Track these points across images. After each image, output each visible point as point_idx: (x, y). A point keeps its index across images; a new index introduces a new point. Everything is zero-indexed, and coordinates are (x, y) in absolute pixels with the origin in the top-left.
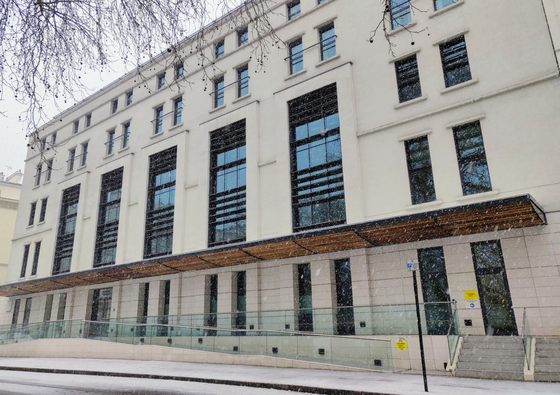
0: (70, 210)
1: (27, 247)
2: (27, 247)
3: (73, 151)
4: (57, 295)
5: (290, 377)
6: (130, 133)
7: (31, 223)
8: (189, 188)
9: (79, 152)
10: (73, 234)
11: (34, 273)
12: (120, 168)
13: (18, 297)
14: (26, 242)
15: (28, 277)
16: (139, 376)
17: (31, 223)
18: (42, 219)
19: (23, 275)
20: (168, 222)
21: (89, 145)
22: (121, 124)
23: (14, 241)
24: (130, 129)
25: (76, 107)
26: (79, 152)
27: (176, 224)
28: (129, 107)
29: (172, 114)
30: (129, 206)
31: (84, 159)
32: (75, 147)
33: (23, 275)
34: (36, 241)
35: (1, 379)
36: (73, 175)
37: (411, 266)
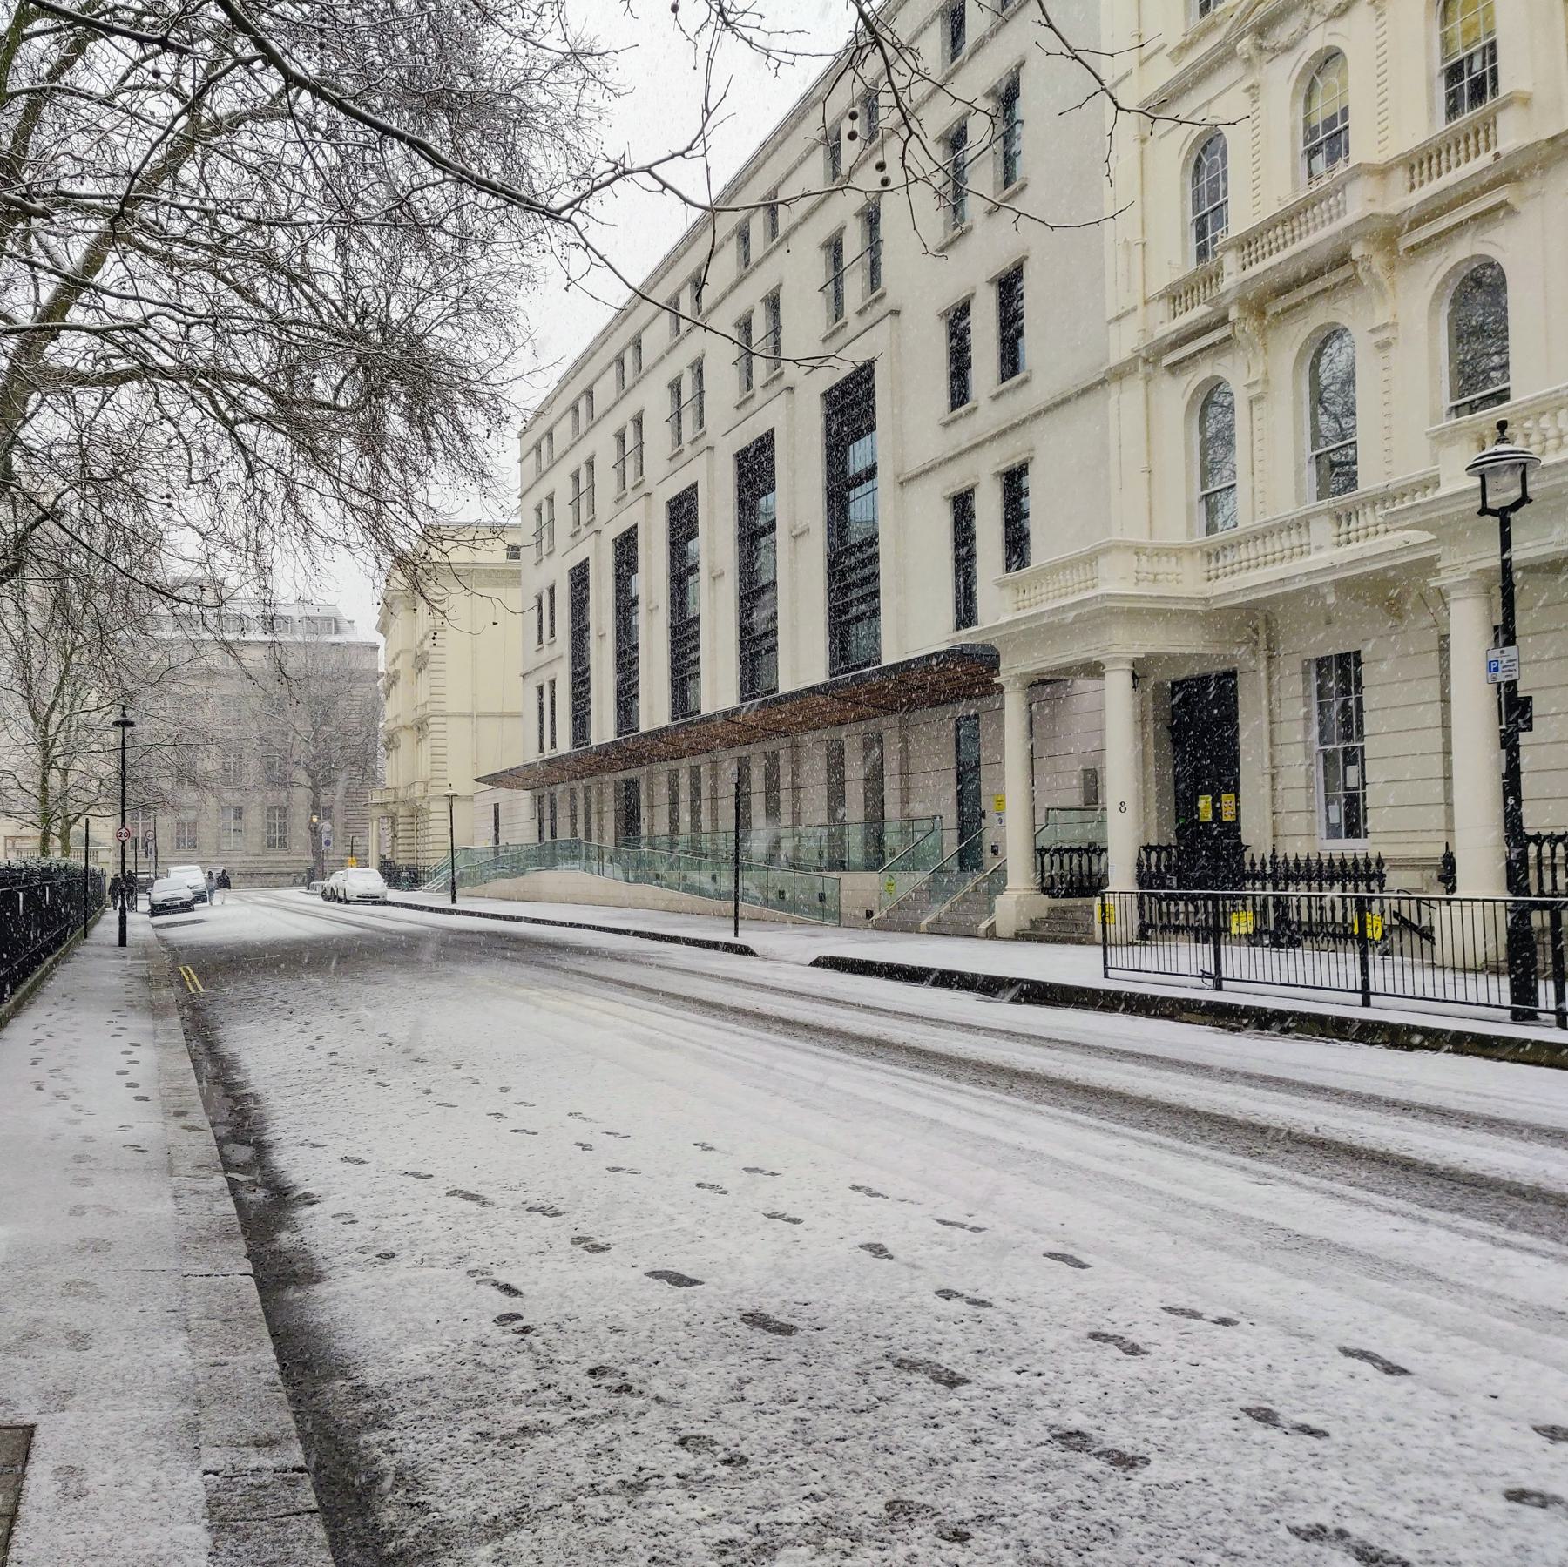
0: (858, 458)
1: (962, 505)
2: (962, 505)
3: (834, 247)
4: (756, 755)
5: (687, 925)
6: (1021, 122)
7: (959, 395)
8: (909, 480)
9: (853, 245)
10: (872, 541)
11: (553, 744)
12: (630, 531)
13: (743, 751)
14: (953, 479)
15: (548, 753)
16: (553, 923)
17: (959, 395)
18: (1010, 361)
19: (541, 749)
20: (865, 581)
21: (1023, 87)
22: (856, 215)
23: (523, 676)
24: (1022, 108)
25: (564, 383)
26: (853, 245)
27: (884, 584)
28: (962, 65)
29: (863, 264)
30: (795, 537)
31: (875, 268)
32: (842, 230)
33: (541, 749)
34: (948, 493)
35: (1559, 1152)
36: (850, 331)
37: (1496, 670)
